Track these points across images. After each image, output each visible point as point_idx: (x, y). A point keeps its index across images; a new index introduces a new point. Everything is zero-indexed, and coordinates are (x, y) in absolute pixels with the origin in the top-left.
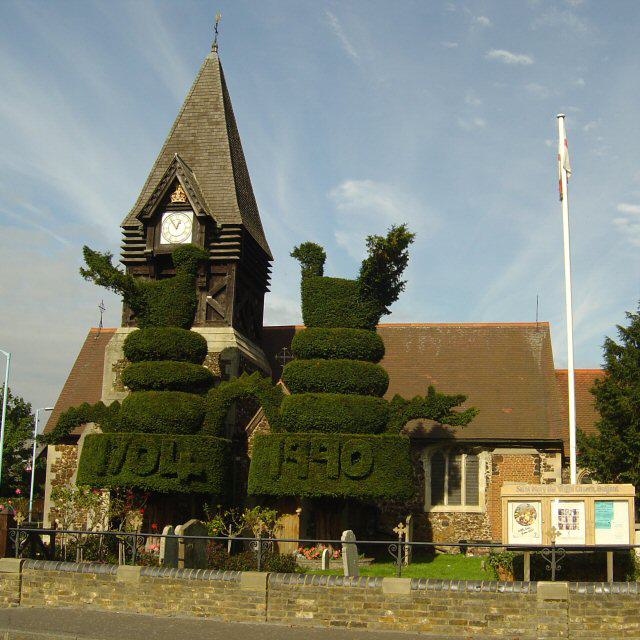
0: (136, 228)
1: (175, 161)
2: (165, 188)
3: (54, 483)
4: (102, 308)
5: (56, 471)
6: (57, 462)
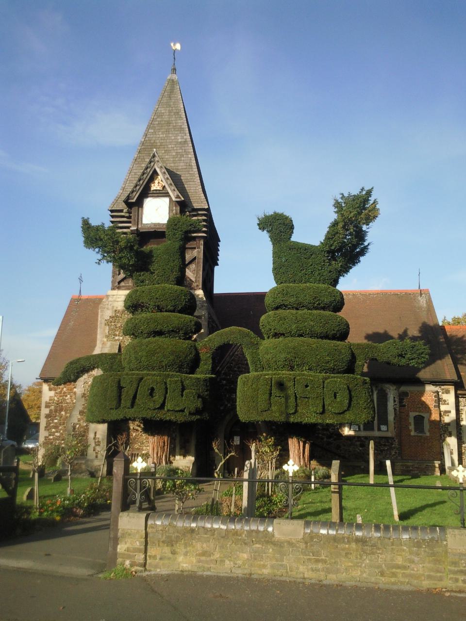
0: (121, 211)
1: (154, 156)
2: (146, 177)
3: (47, 416)
4: (81, 280)
6: (50, 400)
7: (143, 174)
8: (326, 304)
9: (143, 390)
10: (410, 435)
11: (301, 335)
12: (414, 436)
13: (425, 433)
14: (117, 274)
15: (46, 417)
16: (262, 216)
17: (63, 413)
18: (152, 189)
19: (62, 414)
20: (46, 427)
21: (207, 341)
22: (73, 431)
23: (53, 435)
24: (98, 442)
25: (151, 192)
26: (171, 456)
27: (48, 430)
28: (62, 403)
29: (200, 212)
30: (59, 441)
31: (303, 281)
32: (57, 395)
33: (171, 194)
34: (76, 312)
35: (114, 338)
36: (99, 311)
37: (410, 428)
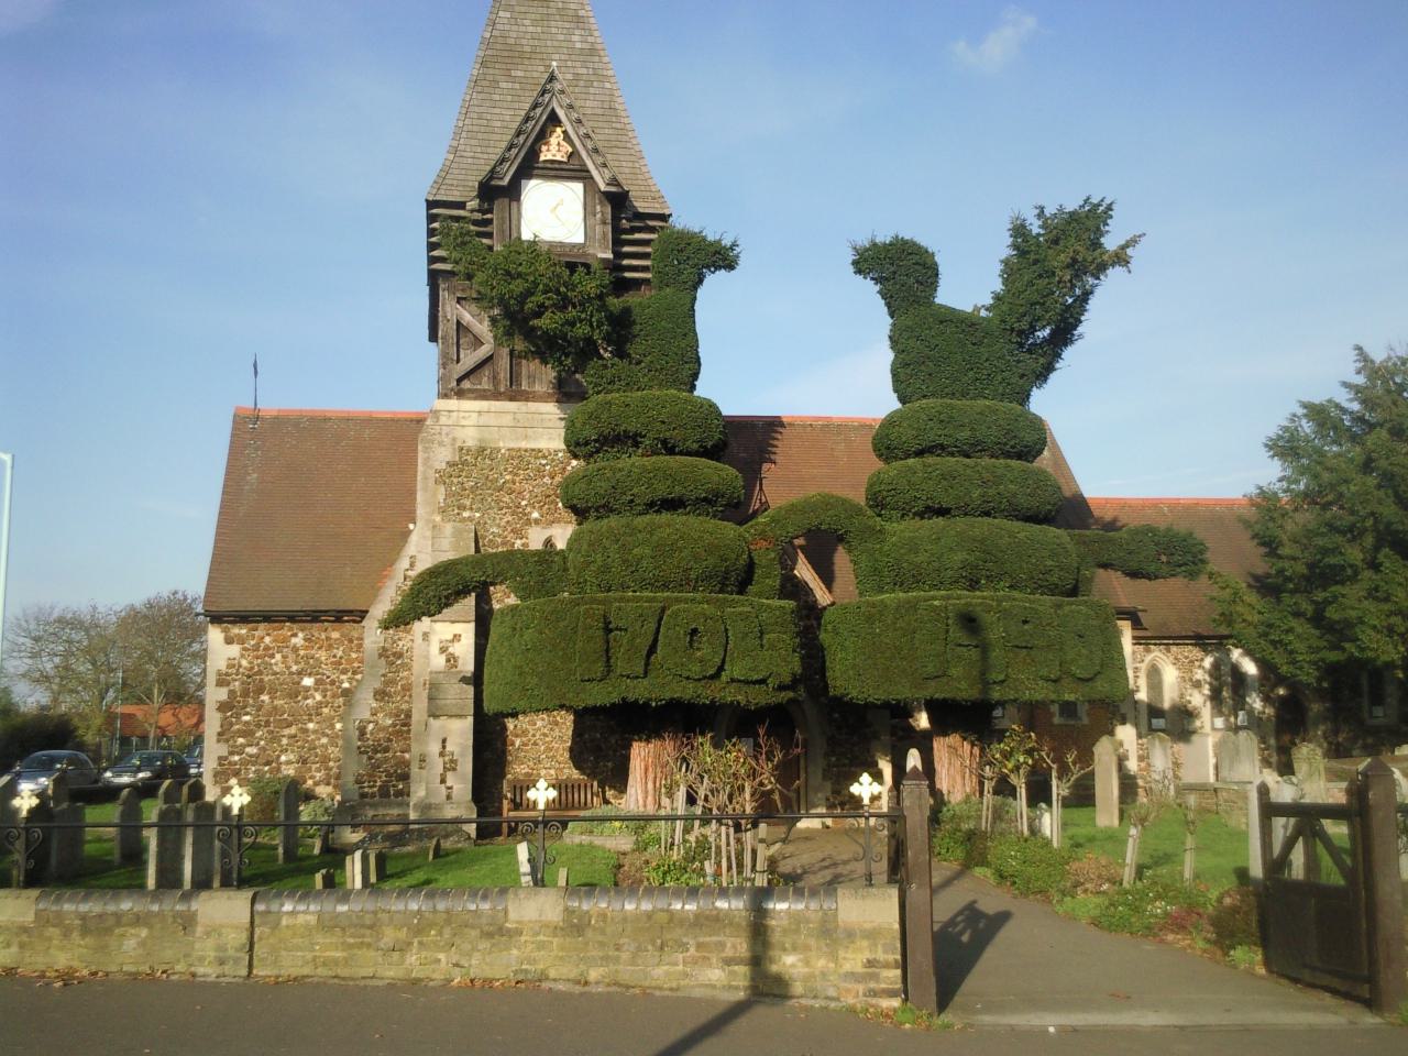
0: (461, 205)
3: (223, 707)
5: (228, 684)
6: (228, 667)
7: (527, 119)
8: (1026, 447)
9: (672, 635)
10: (1052, 725)
11: (987, 514)
12: (1060, 725)
13: (1080, 719)
14: (452, 359)
15: (219, 709)
16: (863, 241)
17: (265, 698)
18: (542, 158)
19: (263, 701)
20: (219, 734)
21: (766, 524)
22: (360, 740)
23: (238, 754)
24: (452, 761)
25: (540, 165)
26: (607, 788)
27: (227, 741)
28: (260, 673)
29: (651, 223)
30: (257, 767)
31: (971, 395)
32: (246, 653)
33: (595, 173)
34: (257, 449)
35: (458, 514)
36: (420, 448)
37: (1052, 710)
